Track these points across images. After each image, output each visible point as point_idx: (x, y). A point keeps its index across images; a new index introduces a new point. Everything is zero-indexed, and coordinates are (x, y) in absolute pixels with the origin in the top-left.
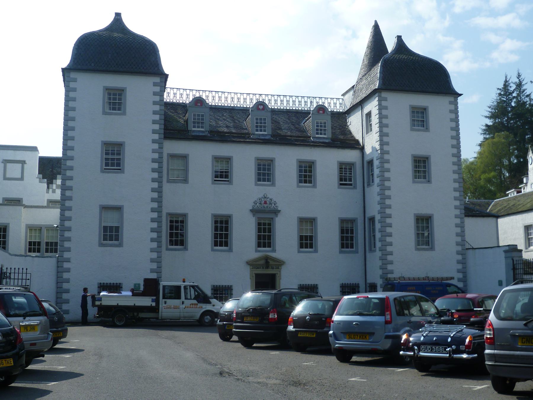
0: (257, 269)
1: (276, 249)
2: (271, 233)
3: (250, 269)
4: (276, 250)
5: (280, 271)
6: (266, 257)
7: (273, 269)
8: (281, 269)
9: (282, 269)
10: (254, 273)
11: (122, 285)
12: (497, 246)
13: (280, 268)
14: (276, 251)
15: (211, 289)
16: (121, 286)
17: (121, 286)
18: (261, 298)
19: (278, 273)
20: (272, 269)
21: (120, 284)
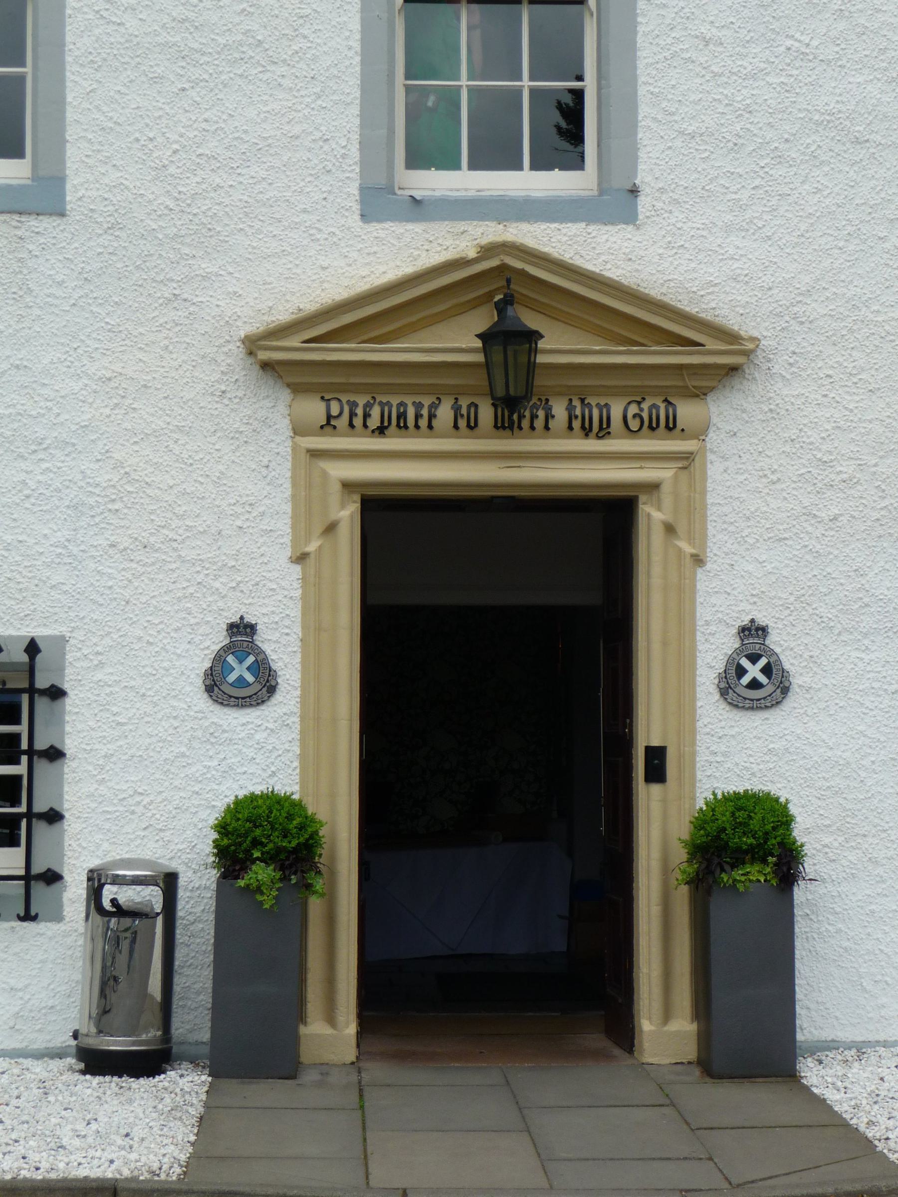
0: (381, 430)
1: (644, 177)
2: (23, 65)
3: (298, 430)
4: (634, 191)
5: (686, 460)
6: (503, 268)
7: (604, 431)
8: (700, 433)
9: (713, 437)
10: (348, 486)
11: (60, 670)
12: (485, 371)
13: (686, 411)
14: (644, 203)
15: (70, 703)
16: (42, 682)
17: (42, 682)
18: (294, 797)
19: (653, 487)
20: (587, 431)
21: (32, 648)
